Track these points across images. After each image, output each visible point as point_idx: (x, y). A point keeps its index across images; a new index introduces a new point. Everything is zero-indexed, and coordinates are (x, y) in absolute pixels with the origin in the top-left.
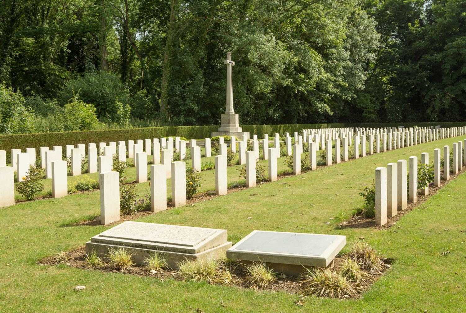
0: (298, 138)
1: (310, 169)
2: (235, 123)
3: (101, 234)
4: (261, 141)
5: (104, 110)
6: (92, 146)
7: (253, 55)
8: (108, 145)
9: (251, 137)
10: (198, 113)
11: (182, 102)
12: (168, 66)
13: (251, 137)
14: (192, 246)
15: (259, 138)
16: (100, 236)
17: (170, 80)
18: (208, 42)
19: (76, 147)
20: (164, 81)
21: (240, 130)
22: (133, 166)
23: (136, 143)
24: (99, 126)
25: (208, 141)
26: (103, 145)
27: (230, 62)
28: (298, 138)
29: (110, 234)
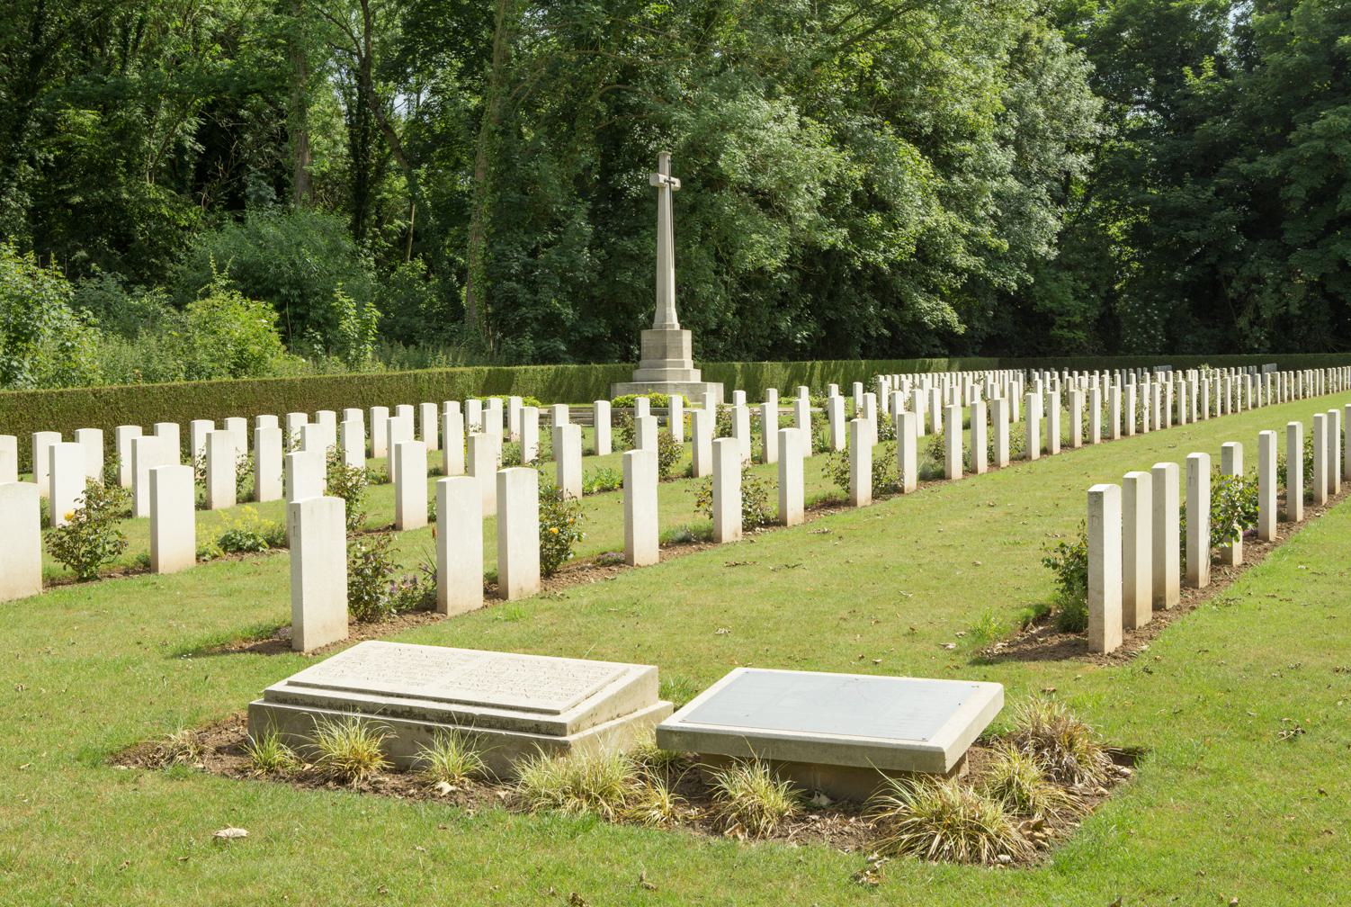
0: (865, 399)
1: (898, 490)
2: (681, 357)
3: (294, 678)
4: (756, 408)
5: (302, 317)
6: (268, 423)
7: (734, 161)
8: (312, 419)
9: (729, 398)
10: (574, 328)
11: (528, 296)
12: (488, 190)
13: (729, 398)
14: (557, 713)
15: (750, 400)
16: (290, 684)
17: (493, 231)
18: (604, 123)
19: (220, 426)
20: (477, 235)
21: (696, 376)
22: (387, 480)
23: (393, 413)
24: (287, 366)
25: (604, 408)
26: (298, 419)
27: (666, 180)
28: (865, 399)
29: (319, 677)
